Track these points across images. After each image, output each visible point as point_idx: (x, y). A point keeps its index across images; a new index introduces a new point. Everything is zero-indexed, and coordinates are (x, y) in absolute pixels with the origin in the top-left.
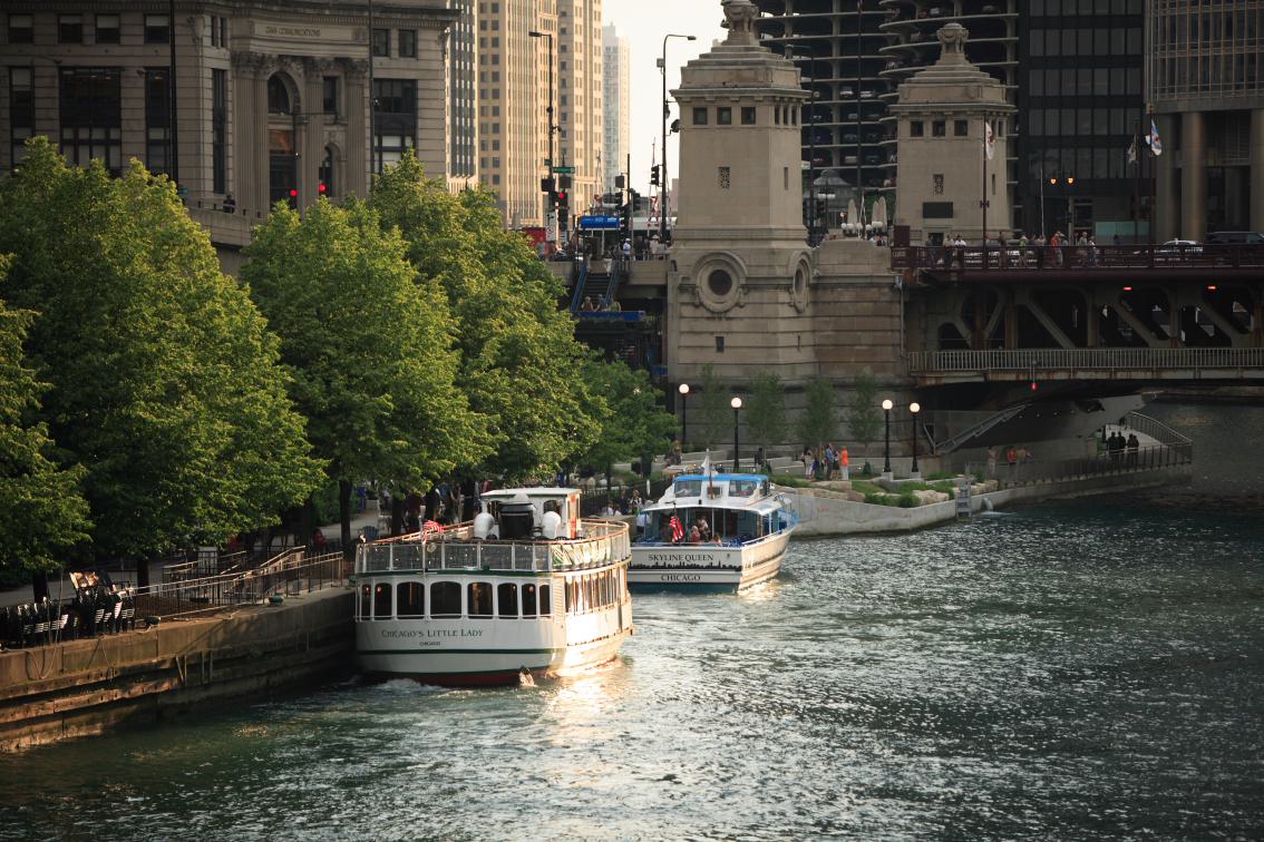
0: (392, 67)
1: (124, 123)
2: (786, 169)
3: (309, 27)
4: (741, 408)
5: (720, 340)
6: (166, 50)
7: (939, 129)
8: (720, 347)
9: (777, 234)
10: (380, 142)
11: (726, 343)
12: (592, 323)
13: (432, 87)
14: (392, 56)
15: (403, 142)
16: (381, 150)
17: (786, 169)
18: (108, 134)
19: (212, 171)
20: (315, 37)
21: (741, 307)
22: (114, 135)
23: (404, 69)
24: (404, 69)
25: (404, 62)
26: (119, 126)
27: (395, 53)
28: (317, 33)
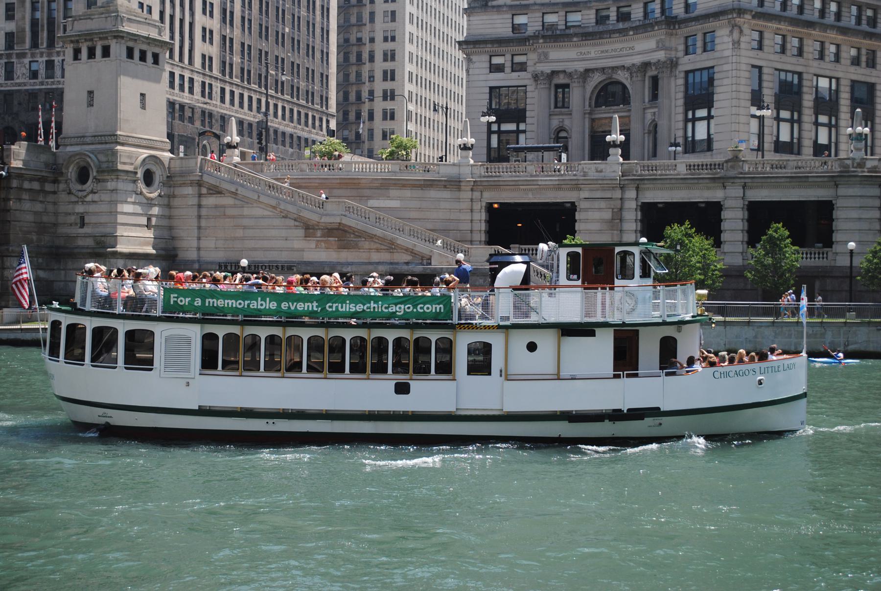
0: (697, 60)
1: (527, 119)
2: (91, 93)
3: (625, 45)
4: (709, 291)
5: (82, 219)
6: (32, 69)
7: (91, 54)
8: (83, 225)
9: (121, 140)
10: (694, 114)
11: (86, 221)
12: (758, 242)
13: (725, 69)
14: (765, 51)
15: (792, 115)
16: (694, 120)
17: (91, 93)
18: (518, 127)
19: (765, 140)
20: (631, 51)
21: (95, 193)
22: (522, 127)
23: (705, 60)
24: (705, 60)
25: (868, 71)
26: (525, 122)
27: (699, 50)
28: (632, 48)
